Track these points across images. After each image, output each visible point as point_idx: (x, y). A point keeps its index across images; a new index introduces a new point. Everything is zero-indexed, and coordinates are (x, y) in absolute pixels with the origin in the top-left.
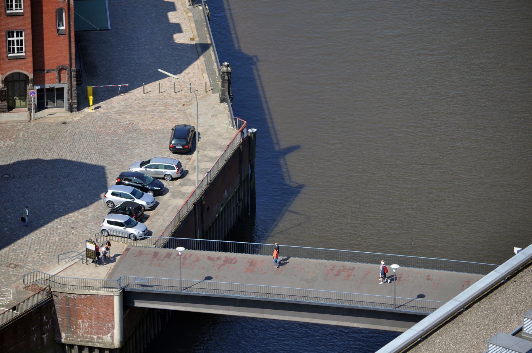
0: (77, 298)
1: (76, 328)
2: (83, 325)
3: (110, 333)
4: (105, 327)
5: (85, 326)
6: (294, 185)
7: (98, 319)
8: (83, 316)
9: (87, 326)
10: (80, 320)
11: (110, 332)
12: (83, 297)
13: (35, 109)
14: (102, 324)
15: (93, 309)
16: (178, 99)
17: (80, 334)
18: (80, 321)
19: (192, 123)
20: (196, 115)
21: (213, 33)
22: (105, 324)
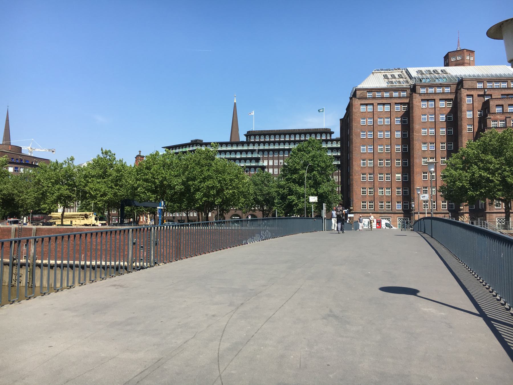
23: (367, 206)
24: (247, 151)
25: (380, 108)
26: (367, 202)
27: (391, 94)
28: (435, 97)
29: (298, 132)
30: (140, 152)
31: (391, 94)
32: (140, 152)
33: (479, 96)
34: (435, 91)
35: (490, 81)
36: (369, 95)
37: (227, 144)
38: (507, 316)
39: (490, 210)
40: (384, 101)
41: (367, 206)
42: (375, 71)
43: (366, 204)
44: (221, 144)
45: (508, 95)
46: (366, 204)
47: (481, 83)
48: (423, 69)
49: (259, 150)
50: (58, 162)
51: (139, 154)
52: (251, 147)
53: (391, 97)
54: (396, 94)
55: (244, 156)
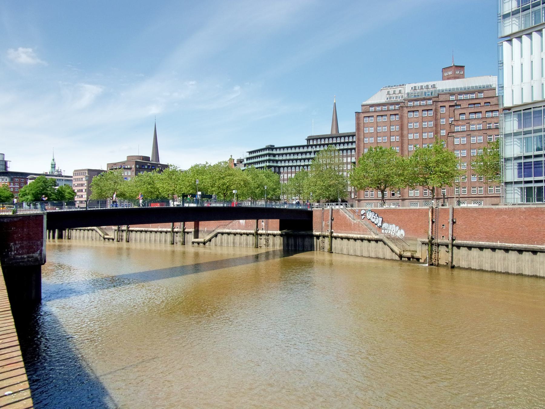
0: (10, 221)
1: (8, 251)
2: (14, 247)
3: (39, 250)
4: (35, 246)
5: (17, 248)
6: (282, 238)
7: (29, 238)
8: (15, 238)
9: (18, 247)
10: (12, 242)
11: (39, 249)
12: (15, 220)
13: (536, 150)
14: (32, 243)
15: (25, 230)
16: (129, 186)
17: (11, 257)
18: (12, 244)
19: (126, 243)
20: (455, 233)
21: (22, 343)
22: (35, 243)
23: (369, 195)
24: (306, 153)
25: (380, 119)
26: (369, 192)
27: (388, 108)
28: (418, 109)
29: (351, 134)
30: (231, 156)
31: (388, 108)
32: (231, 156)
33: (450, 106)
34: (420, 103)
35: (460, 94)
36: (372, 109)
37: (303, 147)
38: (4, 296)
39: (451, 196)
40: (382, 114)
41: (369, 195)
42: (384, 88)
43: (368, 193)
44: (299, 147)
45: (474, 104)
46: (368, 193)
47: (473, 94)
48: (419, 85)
49: (315, 152)
50: (226, 161)
51: (230, 158)
52: (310, 149)
53: (375, 111)
54: (392, 107)
55: (304, 156)
